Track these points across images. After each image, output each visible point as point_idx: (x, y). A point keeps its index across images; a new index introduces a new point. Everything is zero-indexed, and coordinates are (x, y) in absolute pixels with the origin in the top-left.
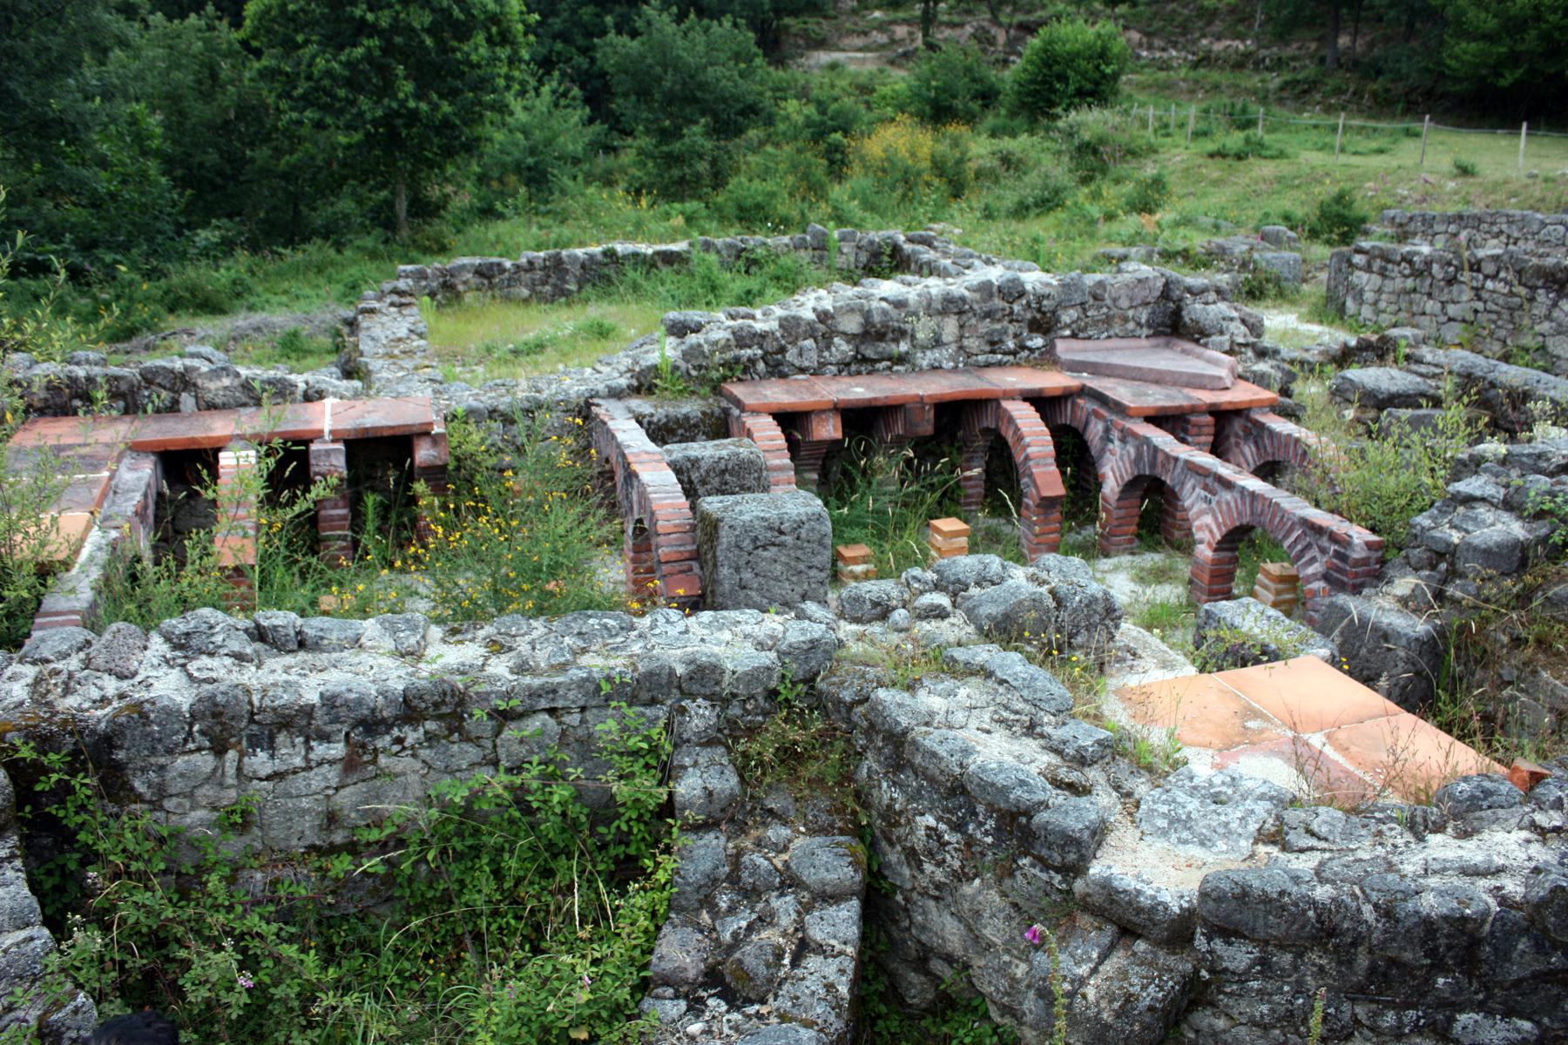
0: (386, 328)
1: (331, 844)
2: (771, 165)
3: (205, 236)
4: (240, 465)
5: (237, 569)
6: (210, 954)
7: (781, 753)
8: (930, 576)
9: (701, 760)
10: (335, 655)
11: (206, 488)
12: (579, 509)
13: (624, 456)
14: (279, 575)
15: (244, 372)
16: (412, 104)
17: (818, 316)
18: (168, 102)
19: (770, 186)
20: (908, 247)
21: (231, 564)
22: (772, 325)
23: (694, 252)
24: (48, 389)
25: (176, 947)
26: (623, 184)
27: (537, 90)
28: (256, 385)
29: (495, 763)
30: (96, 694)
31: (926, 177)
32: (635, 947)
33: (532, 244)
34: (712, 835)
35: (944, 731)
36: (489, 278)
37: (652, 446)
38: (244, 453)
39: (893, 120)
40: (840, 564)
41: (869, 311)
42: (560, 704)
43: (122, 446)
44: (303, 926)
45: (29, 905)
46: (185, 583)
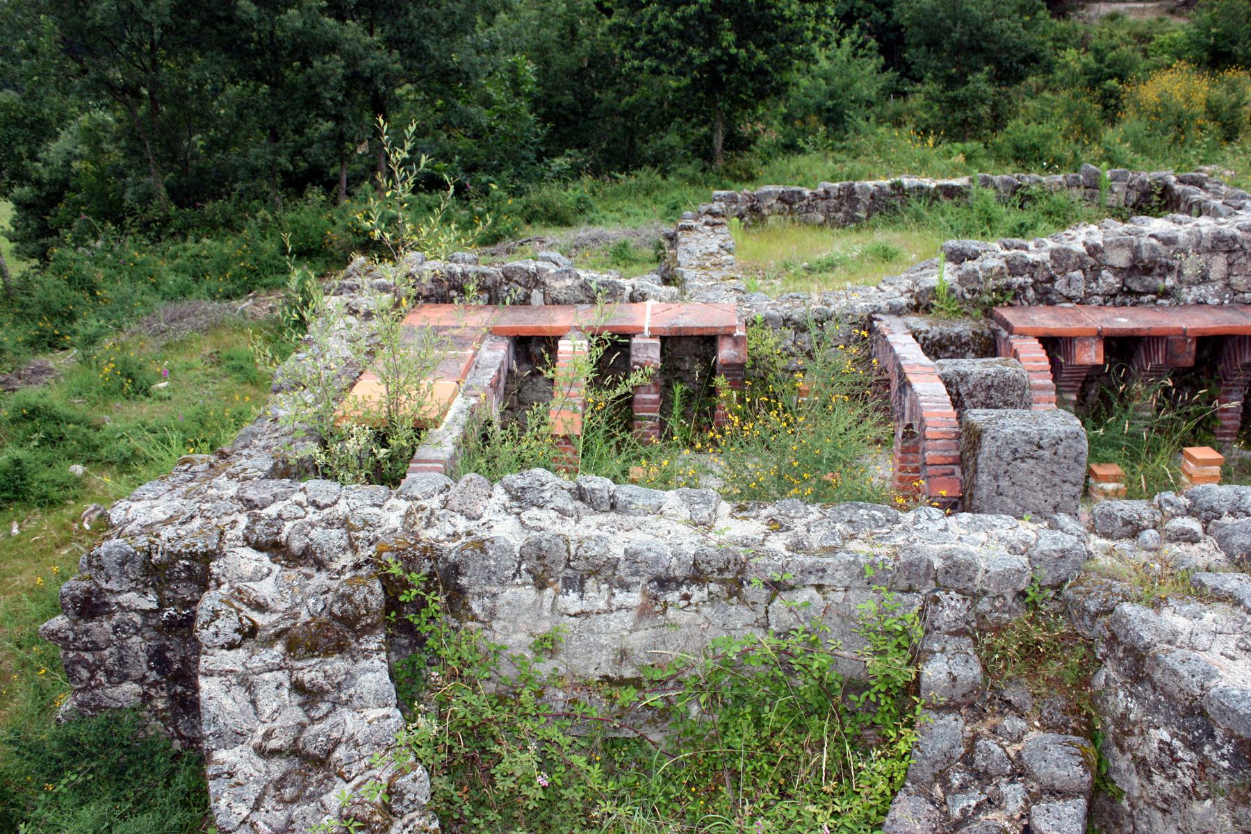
0: (700, 243)
1: (621, 677)
2: (1048, 109)
3: (560, 162)
4: (575, 353)
5: (565, 437)
6: (517, 753)
7: (1023, 650)
8: (1183, 501)
9: (948, 648)
10: (640, 518)
11: (547, 369)
12: (860, 411)
13: (900, 366)
14: (599, 445)
15: (583, 275)
16: (733, 51)
17: (1088, 250)
18: (537, 54)
19: (1046, 128)
20: (1178, 188)
21: (561, 434)
22: (1043, 256)
23: (974, 187)
24: (433, 281)
25: (492, 742)
26: (910, 126)
27: (838, 41)
28: (593, 286)
29: (766, 627)
30: (450, 530)
31: (1200, 122)
32: (872, 807)
33: (828, 176)
34: (952, 717)
35: (1187, 651)
36: (790, 204)
37: (925, 360)
38: (579, 342)
39: (1169, 67)
40: (1092, 481)
41: (1138, 247)
42: (826, 582)
43: (485, 330)
44: (591, 742)
45: (389, 690)
46: (524, 445)
